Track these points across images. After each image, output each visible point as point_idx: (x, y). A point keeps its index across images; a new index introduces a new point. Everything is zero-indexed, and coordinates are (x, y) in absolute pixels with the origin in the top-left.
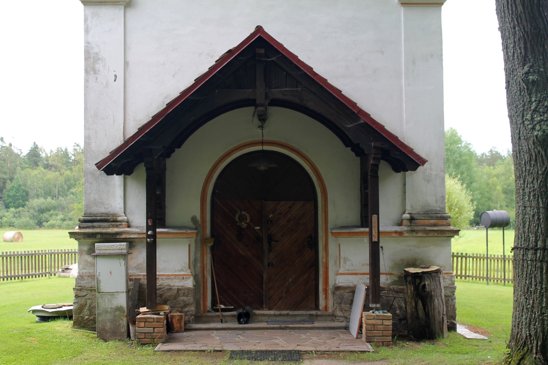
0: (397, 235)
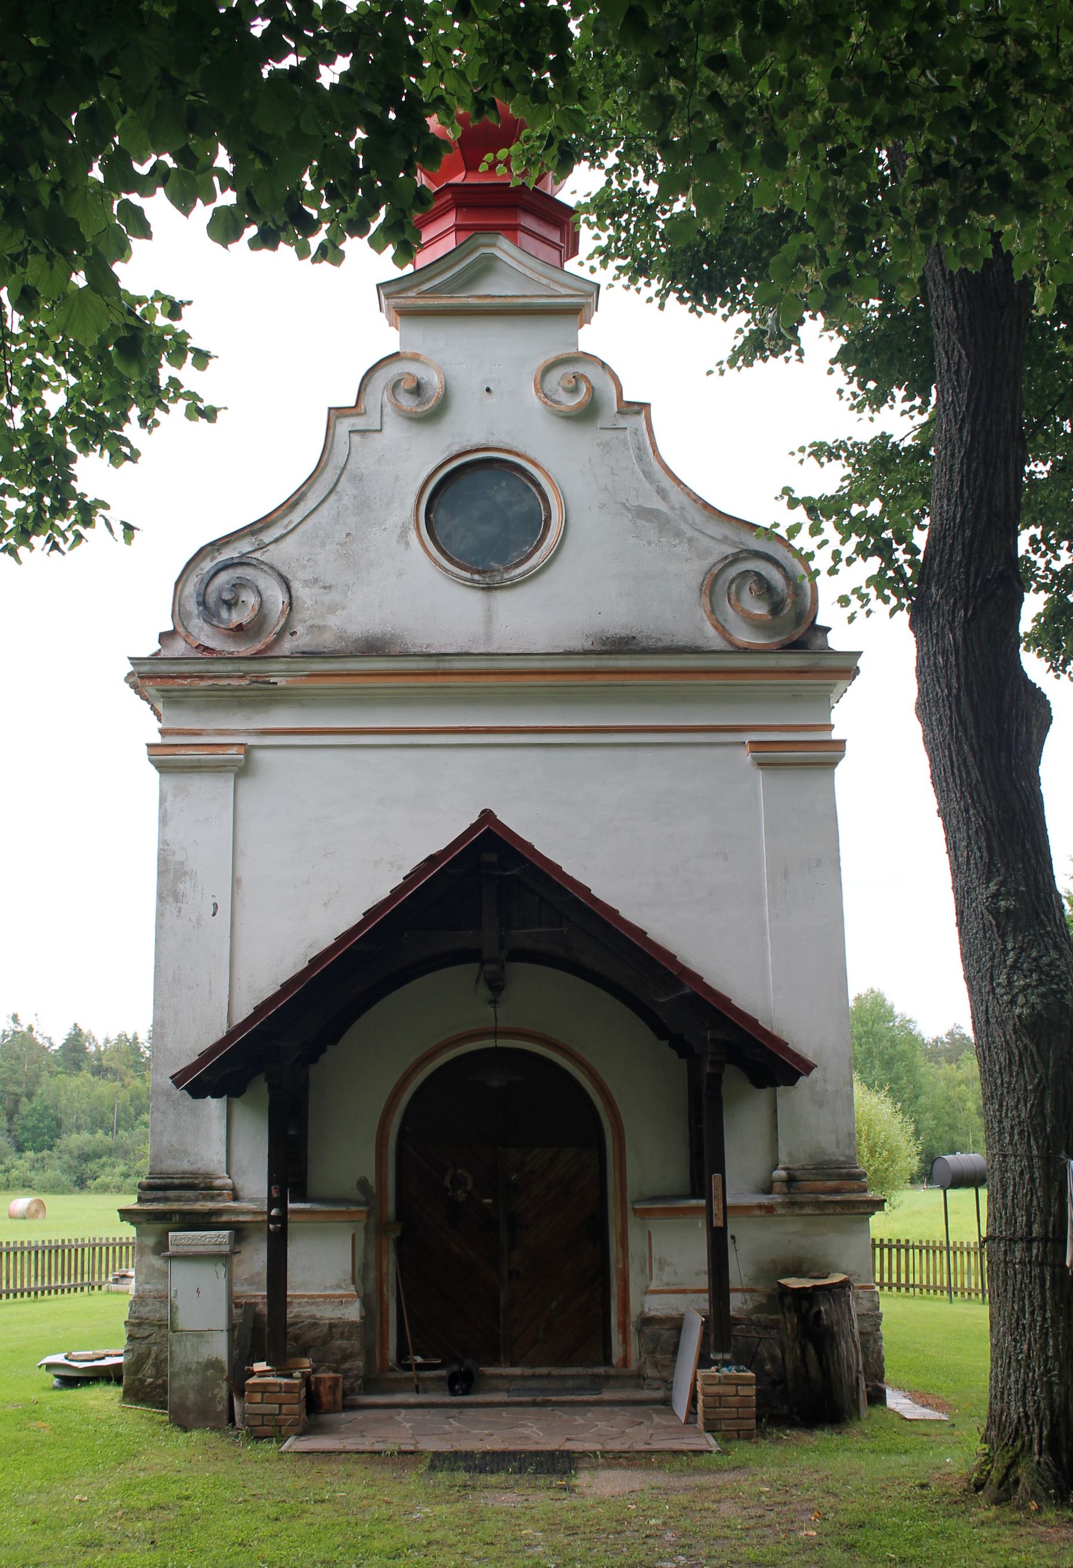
0: (763, 1213)
